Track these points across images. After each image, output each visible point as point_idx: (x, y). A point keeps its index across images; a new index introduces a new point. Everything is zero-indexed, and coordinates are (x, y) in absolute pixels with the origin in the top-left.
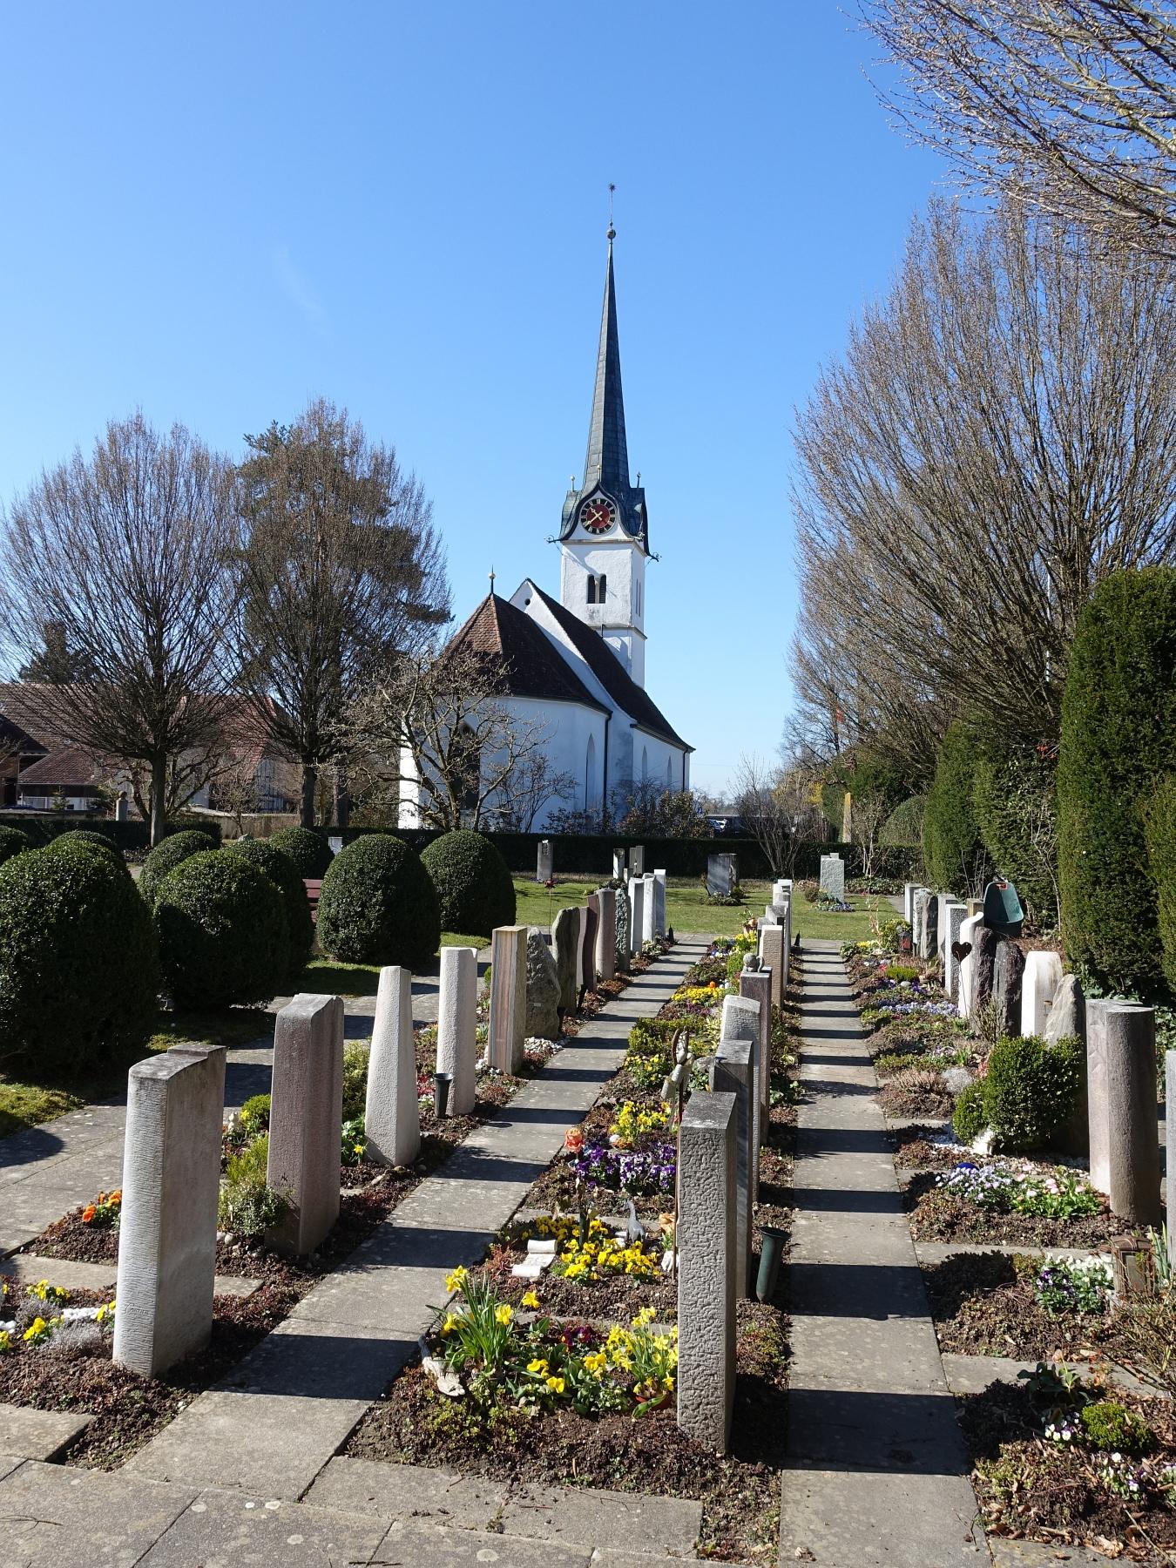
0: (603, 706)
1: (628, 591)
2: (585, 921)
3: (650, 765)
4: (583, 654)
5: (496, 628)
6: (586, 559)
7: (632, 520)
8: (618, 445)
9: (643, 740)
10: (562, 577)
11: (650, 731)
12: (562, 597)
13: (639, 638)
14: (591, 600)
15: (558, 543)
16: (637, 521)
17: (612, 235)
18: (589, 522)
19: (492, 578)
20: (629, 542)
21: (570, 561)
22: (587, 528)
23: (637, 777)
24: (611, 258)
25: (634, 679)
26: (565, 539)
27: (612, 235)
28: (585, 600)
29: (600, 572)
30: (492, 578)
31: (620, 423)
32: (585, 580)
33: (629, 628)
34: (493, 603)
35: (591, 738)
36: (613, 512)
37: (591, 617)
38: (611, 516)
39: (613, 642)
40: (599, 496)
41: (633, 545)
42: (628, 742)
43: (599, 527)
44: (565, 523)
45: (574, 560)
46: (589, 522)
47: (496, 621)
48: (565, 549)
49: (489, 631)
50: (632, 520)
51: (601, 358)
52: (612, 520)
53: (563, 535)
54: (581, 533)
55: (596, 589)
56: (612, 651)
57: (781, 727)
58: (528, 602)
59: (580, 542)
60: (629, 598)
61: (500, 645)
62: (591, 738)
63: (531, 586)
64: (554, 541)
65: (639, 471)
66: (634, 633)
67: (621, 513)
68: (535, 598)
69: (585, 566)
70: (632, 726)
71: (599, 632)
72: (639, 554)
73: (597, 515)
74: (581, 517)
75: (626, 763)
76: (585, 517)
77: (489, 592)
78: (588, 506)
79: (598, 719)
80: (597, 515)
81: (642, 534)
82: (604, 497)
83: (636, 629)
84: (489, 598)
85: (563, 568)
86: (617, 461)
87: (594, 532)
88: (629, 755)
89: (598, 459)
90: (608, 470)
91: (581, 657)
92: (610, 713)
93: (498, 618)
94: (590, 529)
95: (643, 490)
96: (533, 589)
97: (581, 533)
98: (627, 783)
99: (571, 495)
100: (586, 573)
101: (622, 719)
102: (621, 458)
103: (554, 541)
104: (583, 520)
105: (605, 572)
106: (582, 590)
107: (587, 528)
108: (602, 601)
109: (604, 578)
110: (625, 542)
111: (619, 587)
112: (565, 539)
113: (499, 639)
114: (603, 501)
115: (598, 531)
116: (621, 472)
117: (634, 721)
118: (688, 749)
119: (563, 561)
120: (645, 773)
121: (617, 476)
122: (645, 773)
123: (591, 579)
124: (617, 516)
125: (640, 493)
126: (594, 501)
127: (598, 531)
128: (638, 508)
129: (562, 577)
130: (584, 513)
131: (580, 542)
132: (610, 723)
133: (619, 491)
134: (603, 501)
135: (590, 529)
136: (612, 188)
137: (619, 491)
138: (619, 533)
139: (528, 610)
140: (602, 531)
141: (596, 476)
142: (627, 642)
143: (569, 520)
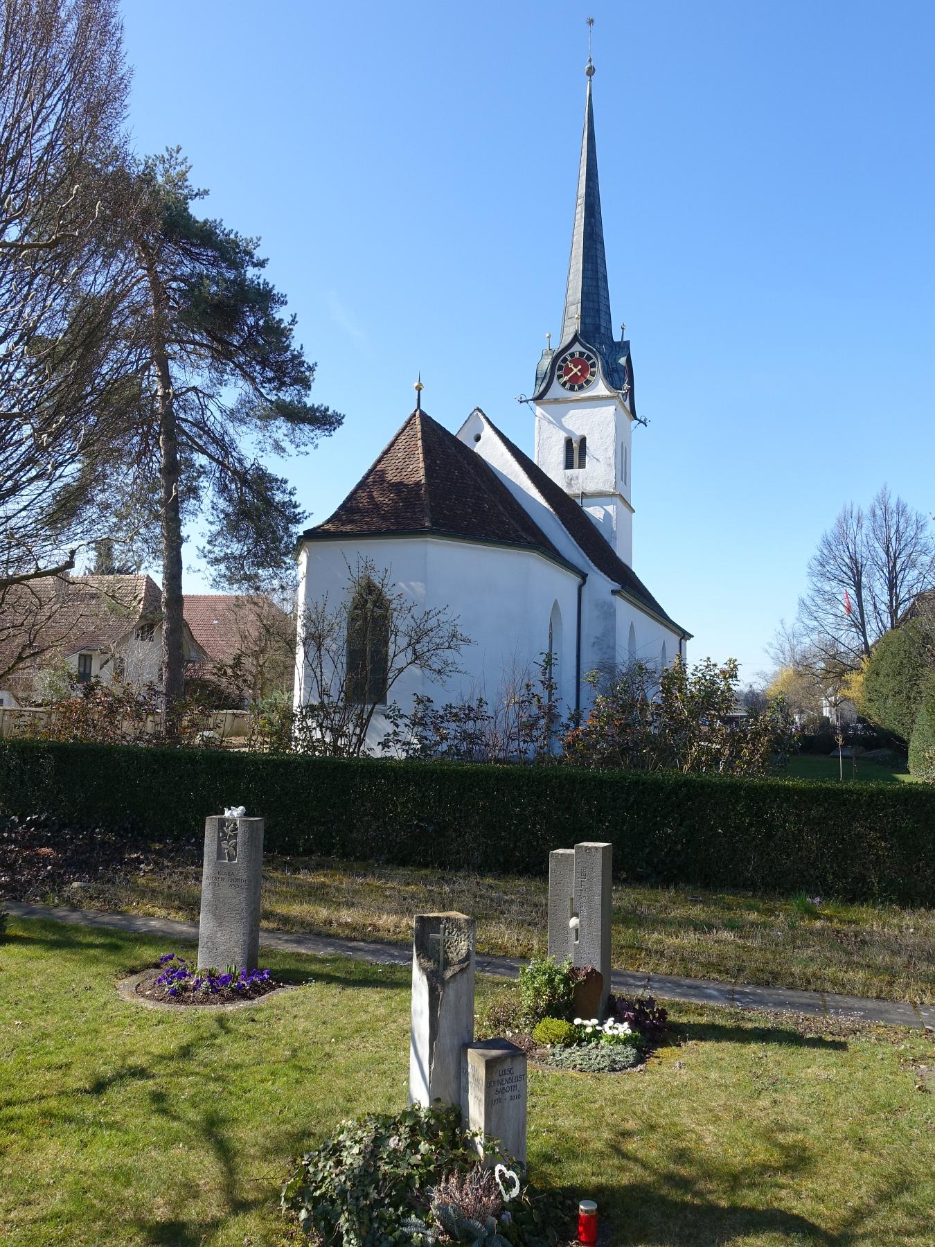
0: (577, 568)
1: (611, 453)
2: (207, 841)
3: (640, 640)
4: (552, 507)
5: (420, 451)
6: (563, 420)
7: (615, 375)
8: (598, 294)
9: (625, 611)
10: (536, 441)
11: (632, 599)
12: (536, 455)
13: (626, 510)
14: (569, 465)
15: (531, 403)
16: (622, 375)
17: (591, 72)
18: (566, 378)
19: (419, 389)
20: (613, 397)
21: (545, 423)
22: (564, 385)
23: (622, 659)
24: (590, 95)
25: (620, 553)
26: (539, 398)
27: (591, 72)
28: (562, 466)
29: (579, 433)
30: (419, 389)
31: (600, 269)
32: (562, 443)
33: (613, 495)
34: (418, 421)
35: (556, 605)
36: (593, 365)
37: (569, 484)
38: (592, 370)
39: (595, 512)
40: (577, 348)
41: (616, 401)
42: (609, 614)
43: (577, 383)
44: (539, 382)
45: (550, 422)
46: (566, 378)
47: (420, 443)
48: (539, 410)
49: (410, 455)
50: (615, 375)
51: (579, 201)
52: (593, 374)
53: (537, 394)
54: (557, 390)
55: (575, 452)
56: (593, 521)
57: (818, 541)
58: (478, 438)
59: (556, 401)
60: (612, 461)
61: (422, 472)
62: (556, 605)
63: (482, 417)
64: (527, 401)
65: (622, 323)
66: (618, 501)
67: (603, 366)
68: (487, 432)
69: (563, 428)
70: (614, 592)
71: (578, 501)
72: (625, 416)
73: (575, 370)
74: (557, 373)
75: (606, 640)
76: (561, 373)
77: (416, 407)
78: (565, 360)
79: (565, 583)
80: (575, 370)
81: (626, 386)
82: (584, 350)
83: (621, 496)
84: (414, 415)
85: (536, 432)
86: (598, 311)
87: (572, 389)
88: (609, 632)
89: (576, 311)
90: (588, 321)
91: (546, 504)
92: (584, 577)
93: (423, 439)
94: (568, 386)
95: (627, 343)
96: (483, 420)
97: (557, 390)
98: (608, 668)
99: (547, 354)
100: (562, 436)
101: (601, 583)
102: (602, 308)
103: (527, 401)
104: (559, 377)
105: (585, 433)
106: (559, 454)
107: (564, 385)
108: (582, 466)
109: (583, 440)
110: (607, 398)
111: (601, 450)
112: (539, 398)
113: (422, 465)
114: (582, 354)
115: (576, 388)
116: (603, 323)
117: (616, 586)
118: (685, 635)
119: (537, 423)
120: (632, 653)
121: (597, 328)
122: (632, 653)
123: (569, 442)
124: (599, 369)
125: (624, 347)
126: (572, 355)
127: (576, 388)
128: (623, 361)
129: (536, 441)
130: (560, 368)
131: (556, 401)
132: (584, 589)
133: (601, 344)
134: (582, 354)
135: (568, 386)
136: (591, 22)
137: (601, 344)
138: (600, 388)
139: (478, 449)
140: (581, 387)
141: (573, 327)
142: (611, 512)
143: (544, 378)
